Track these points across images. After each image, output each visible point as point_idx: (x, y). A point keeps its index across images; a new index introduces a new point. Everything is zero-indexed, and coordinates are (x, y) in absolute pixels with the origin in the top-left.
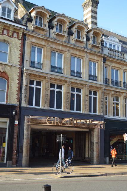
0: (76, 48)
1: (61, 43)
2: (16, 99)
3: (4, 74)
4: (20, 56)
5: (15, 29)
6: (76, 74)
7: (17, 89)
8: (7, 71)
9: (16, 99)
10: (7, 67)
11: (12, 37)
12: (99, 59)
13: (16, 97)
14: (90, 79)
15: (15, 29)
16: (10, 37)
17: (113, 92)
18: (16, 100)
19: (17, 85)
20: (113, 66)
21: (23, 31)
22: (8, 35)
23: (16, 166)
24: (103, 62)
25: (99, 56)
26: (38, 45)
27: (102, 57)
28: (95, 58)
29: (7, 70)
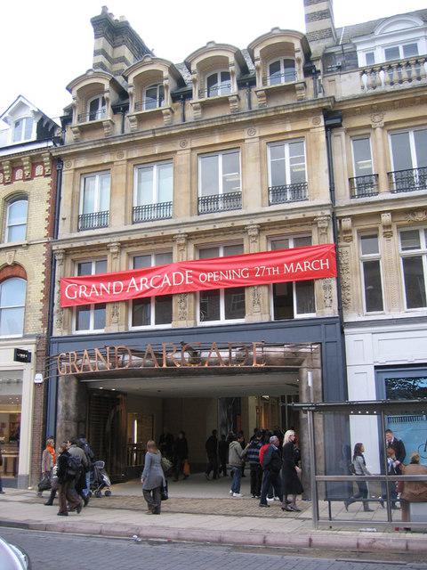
0: (199, 127)
1: (151, 136)
2: (40, 320)
3: (18, 268)
4: (47, 214)
5: (32, 157)
6: (221, 205)
7: (42, 296)
8: (19, 259)
9: (40, 320)
10: (19, 250)
11: (33, 175)
12: (308, 124)
13: (40, 315)
14: (352, 197)
15: (32, 157)
16: (9, 183)
17: (386, 218)
18: (40, 324)
19: (42, 287)
20: (387, 124)
21: (48, 154)
22: (25, 179)
23: (214, 478)
24: (323, 129)
25: (300, 115)
26: (95, 169)
27: (313, 113)
28: (289, 128)
29: (20, 257)
